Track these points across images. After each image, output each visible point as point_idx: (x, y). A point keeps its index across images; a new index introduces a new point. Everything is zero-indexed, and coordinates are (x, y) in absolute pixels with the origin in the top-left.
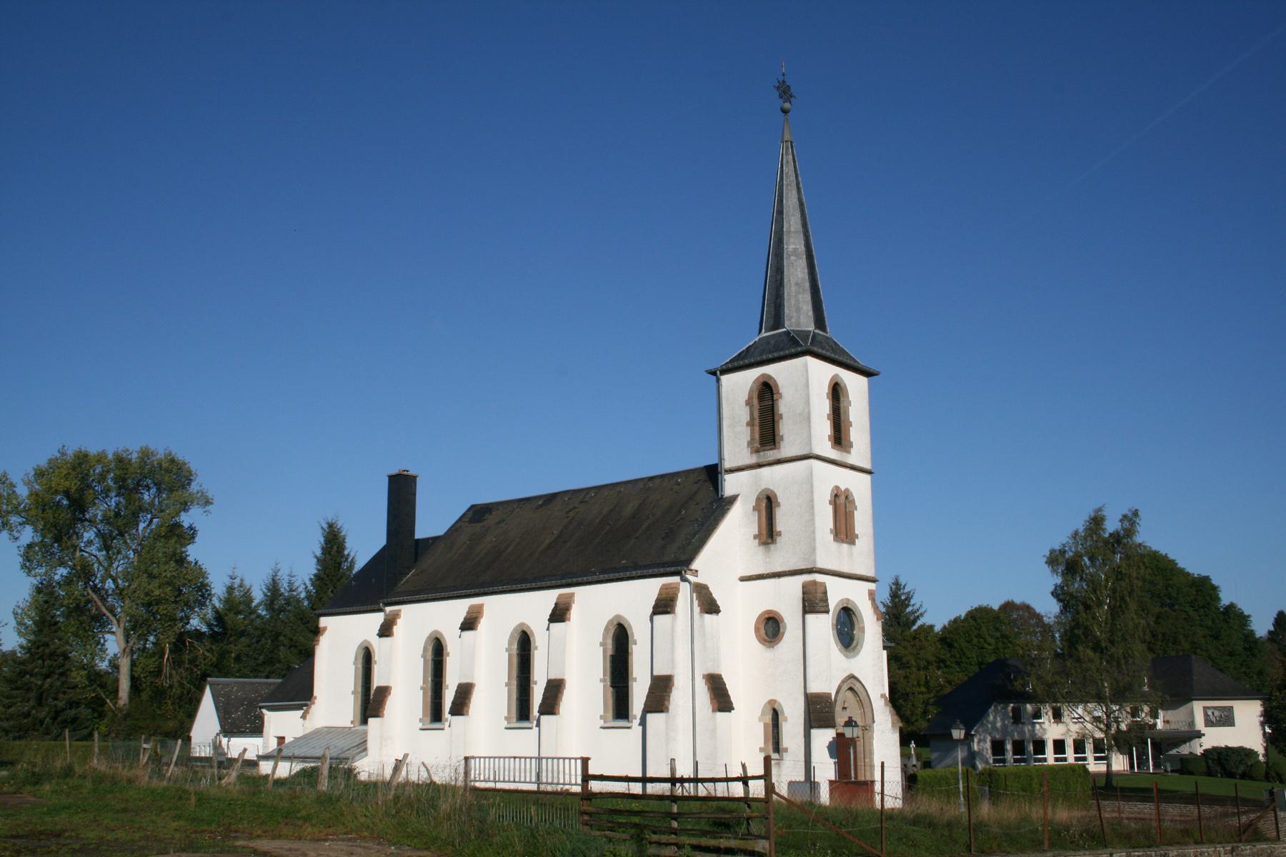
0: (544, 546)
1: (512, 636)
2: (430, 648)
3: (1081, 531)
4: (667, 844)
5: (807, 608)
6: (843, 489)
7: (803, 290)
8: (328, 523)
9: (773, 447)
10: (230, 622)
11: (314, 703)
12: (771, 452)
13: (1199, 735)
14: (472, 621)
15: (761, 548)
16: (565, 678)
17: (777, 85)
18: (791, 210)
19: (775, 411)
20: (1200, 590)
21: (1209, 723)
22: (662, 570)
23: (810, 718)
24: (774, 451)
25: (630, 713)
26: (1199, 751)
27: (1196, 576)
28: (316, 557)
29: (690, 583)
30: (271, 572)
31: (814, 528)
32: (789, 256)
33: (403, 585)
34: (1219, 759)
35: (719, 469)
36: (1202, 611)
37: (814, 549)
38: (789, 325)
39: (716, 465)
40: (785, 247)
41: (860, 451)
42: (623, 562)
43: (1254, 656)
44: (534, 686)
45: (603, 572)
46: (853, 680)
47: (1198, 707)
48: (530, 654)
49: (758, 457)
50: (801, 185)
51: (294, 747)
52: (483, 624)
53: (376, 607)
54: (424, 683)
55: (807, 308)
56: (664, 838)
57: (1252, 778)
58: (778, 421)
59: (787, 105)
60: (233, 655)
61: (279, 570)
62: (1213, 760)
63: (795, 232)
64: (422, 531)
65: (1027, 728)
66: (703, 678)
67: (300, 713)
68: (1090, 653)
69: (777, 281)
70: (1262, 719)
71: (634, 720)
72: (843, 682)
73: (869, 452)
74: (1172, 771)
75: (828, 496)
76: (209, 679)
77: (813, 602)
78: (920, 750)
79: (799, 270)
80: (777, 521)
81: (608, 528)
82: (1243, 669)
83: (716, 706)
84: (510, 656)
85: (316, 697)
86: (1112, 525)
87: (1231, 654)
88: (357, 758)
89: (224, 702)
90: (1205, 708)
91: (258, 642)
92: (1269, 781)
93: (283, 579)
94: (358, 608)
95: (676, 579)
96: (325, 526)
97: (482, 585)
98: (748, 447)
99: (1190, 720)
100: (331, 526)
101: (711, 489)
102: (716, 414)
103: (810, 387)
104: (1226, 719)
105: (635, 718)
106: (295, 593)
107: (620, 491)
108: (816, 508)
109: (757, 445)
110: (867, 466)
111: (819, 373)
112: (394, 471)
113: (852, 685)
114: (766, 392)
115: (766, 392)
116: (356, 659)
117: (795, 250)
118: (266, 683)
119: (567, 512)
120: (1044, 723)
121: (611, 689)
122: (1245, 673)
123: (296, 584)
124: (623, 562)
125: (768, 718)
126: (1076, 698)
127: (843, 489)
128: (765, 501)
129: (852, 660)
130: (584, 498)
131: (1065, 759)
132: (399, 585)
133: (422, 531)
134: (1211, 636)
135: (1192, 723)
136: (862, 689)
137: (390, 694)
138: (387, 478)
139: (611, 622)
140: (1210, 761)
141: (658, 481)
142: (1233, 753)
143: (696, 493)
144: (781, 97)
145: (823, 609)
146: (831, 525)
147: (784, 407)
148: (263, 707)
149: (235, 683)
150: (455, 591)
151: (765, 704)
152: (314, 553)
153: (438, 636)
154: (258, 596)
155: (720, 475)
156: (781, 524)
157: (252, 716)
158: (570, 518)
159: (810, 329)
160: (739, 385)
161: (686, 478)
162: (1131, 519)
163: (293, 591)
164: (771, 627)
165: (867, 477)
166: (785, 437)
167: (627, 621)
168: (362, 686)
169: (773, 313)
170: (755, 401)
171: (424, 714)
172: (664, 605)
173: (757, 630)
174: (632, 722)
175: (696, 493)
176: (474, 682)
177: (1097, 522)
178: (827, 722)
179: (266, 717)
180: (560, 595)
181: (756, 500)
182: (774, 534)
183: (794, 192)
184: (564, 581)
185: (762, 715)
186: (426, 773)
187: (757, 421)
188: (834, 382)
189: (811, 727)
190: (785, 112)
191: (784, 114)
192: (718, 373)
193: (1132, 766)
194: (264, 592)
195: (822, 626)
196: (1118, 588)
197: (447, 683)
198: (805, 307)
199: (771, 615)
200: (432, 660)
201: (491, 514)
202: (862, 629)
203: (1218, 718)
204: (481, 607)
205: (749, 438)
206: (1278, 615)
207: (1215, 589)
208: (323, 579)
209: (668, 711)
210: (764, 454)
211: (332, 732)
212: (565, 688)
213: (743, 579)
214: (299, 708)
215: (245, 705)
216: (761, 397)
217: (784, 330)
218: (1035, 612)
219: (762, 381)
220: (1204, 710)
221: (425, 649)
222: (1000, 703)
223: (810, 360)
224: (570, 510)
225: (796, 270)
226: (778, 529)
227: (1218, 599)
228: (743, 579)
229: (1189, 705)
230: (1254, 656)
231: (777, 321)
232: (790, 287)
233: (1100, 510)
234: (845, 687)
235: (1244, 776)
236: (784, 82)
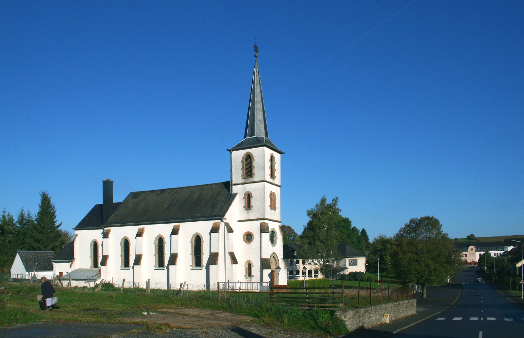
0: (164, 208)
1: (156, 239)
2: (123, 242)
3: (318, 204)
4: (305, 306)
5: (262, 231)
6: (273, 192)
7: (262, 123)
8: (43, 193)
9: (251, 177)
10: (5, 229)
11: (74, 260)
12: (250, 179)
13: (347, 268)
14: (141, 233)
15: (246, 211)
16: (178, 253)
17: (254, 46)
18: (258, 93)
19: (252, 165)
20: (346, 223)
21: (350, 264)
22: (214, 218)
23: (263, 266)
24: (251, 179)
25: (202, 265)
26: (347, 273)
27: (344, 218)
28: (39, 205)
29: (224, 222)
30: (21, 211)
31: (265, 205)
32: (257, 111)
33: (110, 220)
34: (353, 275)
35: (231, 184)
36: (346, 229)
37: (265, 212)
38: (257, 135)
39: (229, 182)
40: (256, 107)
41: (278, 181)
42: (198, 215)
43: (360, 243)
44: (165, 256)
45: (191, 218)
46: (274, 254)
47: (347, 260)
48: (163, 245)
49: (245, 181)
50: (261, 85)
51: (78, 276)
52: (145, 234)
53: (101, 227)
54: (121, 254)
55: (263, 129)
56: (304, 304)
57: (363, 281)
58: (253, 169)
59: (257, 54)
60: (7, 241)
61: (24, 210)
62: (351, 276)
63: (259, 102)
64: (116, 200)
65: (294, 267)
67: (69, 264)
68: (320, 243)
69: (252, 119)
70: (365, 263)
71: (203, 267)
72: (272, 255)
73: (280, 180)
74: (339, 279)
75: (269, 195)
76: (18, 251)
77: (264, 229)
78: (377, 279)
79: (260, 115)
80: (252, 202)
81: (189, 202)
82: (357, 247)
83: (233, 262)
84: (155, 246)
85: (75, 259)
86: (329, 201)
87: (353, 243)
88: (98, 279)
89: (25, 259)
90: (349, 260)
91: (17, 236)
92: (368, 282)
93: (26, 213)
94: (91, 228)
95: (219, 221)
96: (42, 194)
97: (143, 221)
99: (345, 264)
100: (44, 194)
101: (227, 190)
102: (229, 164)
103: (265, 157)
104: (355, 263)
105: (204, 266)
106: (31, 218)
107: (191, 190)
108: (266, 198)
109: (245, 176)
110: (279, 184)
111: (268, 152)
112: (105, 180)
113: (274, 255)
116: (91, 245)
117: (259, 108)
118: (34, 252)
119: (171, 196)
120: (299, 265)
121: (194, 257)
122: (357, 249)
123: (31, 215)
124: (198, 215)
125: (247, 266)
126: (313, 257)
127: (273, 192)
128: (247, 195)
129: (274, 248)
130: (177, 191)
132: (109, 220)
133: (116, 200)
134: (347, 237)
135: (345, 265)
136: (276, 257)
137: (108, 258)
138: (102, 182)
139: (194, 235)
140: (351, 276)
141: (205, 187)
142: (358, 274)
143: (221, 191)
144: (255, 51)
145: (267, 232)
147: (255, 164)
148: (53, 262)
149: (28, 252)
151: (246, 262)
152: (38, 204)
153: (126, 238)
154: (16, 219)
155: (231, 186)
156: (253, 202)
158: (172, 198)
159: (264, 137)
160: (238, 155)
161: (216, 186)
162: (335, 200)
163: (30, 217)
164: (249, 237)
165: (279, 188)
166: (255, 174)
167: (200, 234)
168: (94, 255)
169: (251, 130)
170: (244, 161)
171: (246, 273)
172: (215, 230)
173: (244, 238)
174: (203, 267)
175: (221, 191)
176: (142, 254)
177: (323, 201)
178: (268, 267)
179: (54, 265)
180: (175, 225)
182: (251, 206)
183: (259, 87)
184: (177, 221)
185: (245, 265)
186: (388, 294)
187: (245, 168)
189: (263, 269)
190: (256, 57)
191: (255, 58)
192: (231, 150)
193: (325, 277)
194: (18, 218)
195: (266, 237)
196: (330, 223)
197: (131, 254)
198: (262, 129)
199: (249, 233)
200: (124, 246)
201: (140, 196)
202: (277, 238)
204: (143, 229)
205: (242, 174)
206: (362, 230)
207: (350, 222)
208: (43, 213)
209: (217, 264)
211: (82, 271)
212: (178, 256)
213: (239, 221)
214: (69, 262)
216: (246, 160)
217: (255, 137)
218: (292, 229)
219: (247, 154)
221: (121, 243)
222: (286, 259)
223: (265, 148)
224: (172, 196)
225: (259, 115)
226: (252, 205)
227: (351, 225)
228: (239, 221)
229: (345, 259)
230: (360, 243)
231: (253, 133)
232: (257, 121)
233: (324, 197)
234: (272, 256)
235: (360, 280)
236: (256, 45)
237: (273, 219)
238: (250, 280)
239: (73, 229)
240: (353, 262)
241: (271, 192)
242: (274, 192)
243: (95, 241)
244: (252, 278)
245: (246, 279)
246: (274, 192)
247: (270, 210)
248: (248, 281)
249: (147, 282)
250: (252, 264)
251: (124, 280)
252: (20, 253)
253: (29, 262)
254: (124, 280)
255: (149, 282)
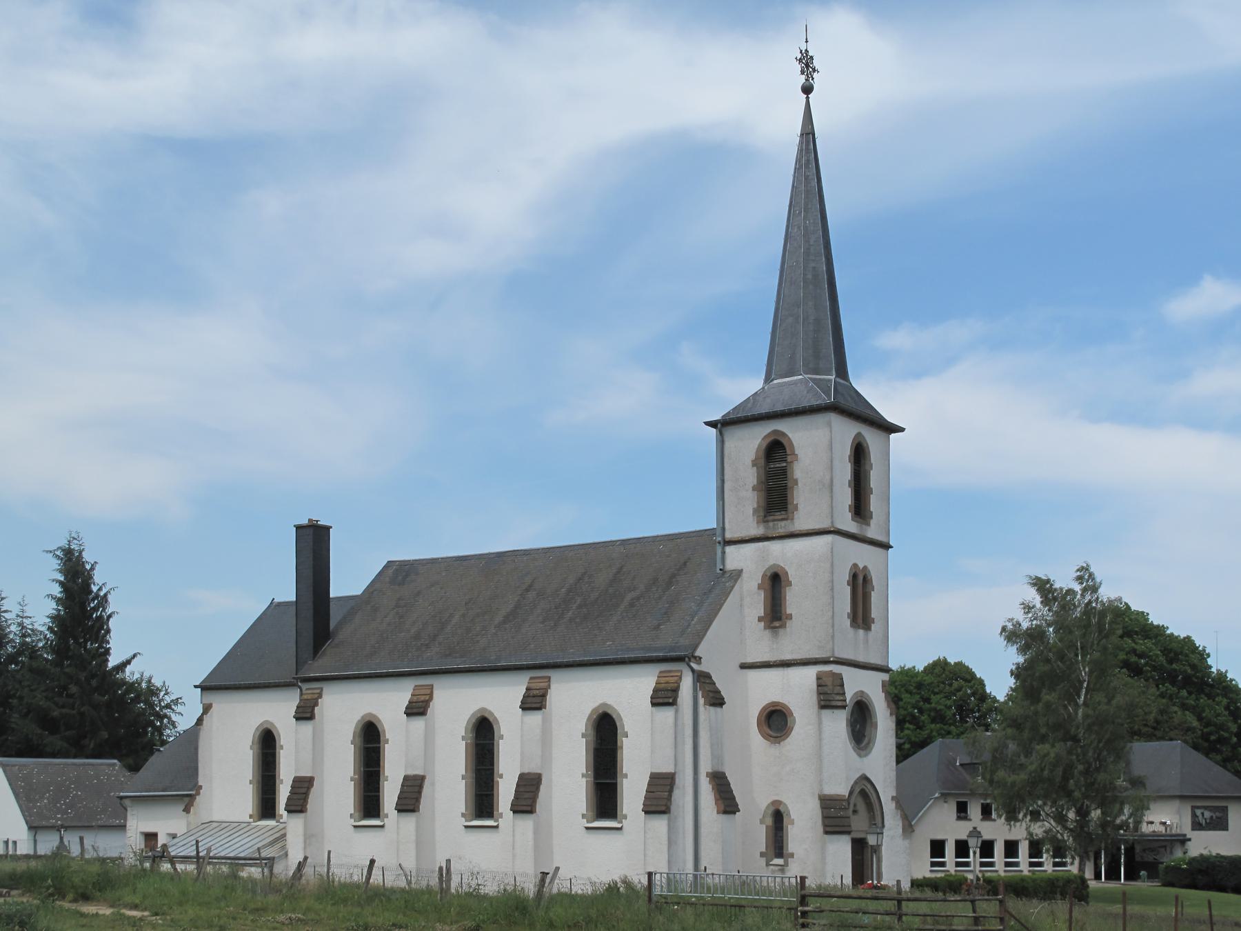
6: (861, 566)
12: (783, 523)
66: (707, 776)
72: (856, 783)
75: (846, 577)
77: (829, 696)
98: (753, 515)
114: (776, 451)
115: (776, 451)
127: (861, 566)
129: (865, 760)
131: (1017, 864)
145: (840, 704)
146: (848, 610)
150: (1088, 685)
151: (769, 804)
156: (793, 601)
157: (62, 805)
181: (762, 576)
188: (857, 442)
195: (837, 723)
199: (778, 708)
203: (1208, 821)
210: (774, 525)
215: (51, 791)
220: (1192, 809)
234: (857, 790)
236: (806, 50)
237: (861, 658)
238: (780, 870)
239: (196, 687)
240: (1207, 814)
241: (855, 565)
242: (865, 567)
243: (269, 727)
244: (786, 864)
245: (768, 865)
246: (865, 567)
247: (851, 631)
248: (773, 872)
249: (441, 869)
250: (789, 814)
251: (372, 862)
252: (8, 765)
253: (37, 797)
254: (372, 862)
255: (448, 870)
